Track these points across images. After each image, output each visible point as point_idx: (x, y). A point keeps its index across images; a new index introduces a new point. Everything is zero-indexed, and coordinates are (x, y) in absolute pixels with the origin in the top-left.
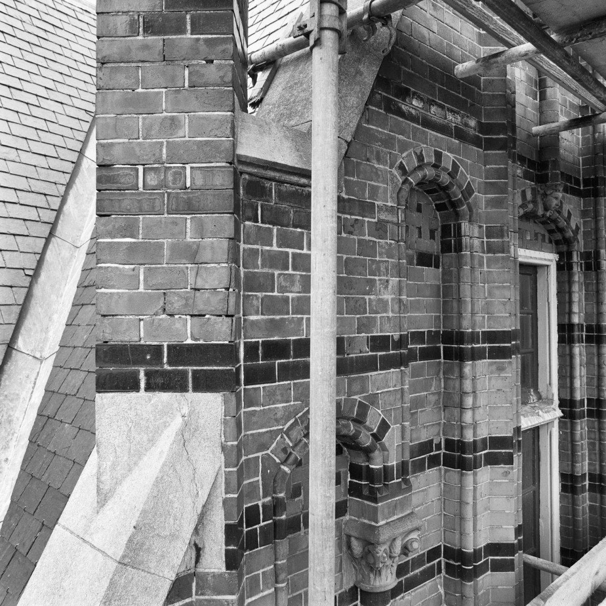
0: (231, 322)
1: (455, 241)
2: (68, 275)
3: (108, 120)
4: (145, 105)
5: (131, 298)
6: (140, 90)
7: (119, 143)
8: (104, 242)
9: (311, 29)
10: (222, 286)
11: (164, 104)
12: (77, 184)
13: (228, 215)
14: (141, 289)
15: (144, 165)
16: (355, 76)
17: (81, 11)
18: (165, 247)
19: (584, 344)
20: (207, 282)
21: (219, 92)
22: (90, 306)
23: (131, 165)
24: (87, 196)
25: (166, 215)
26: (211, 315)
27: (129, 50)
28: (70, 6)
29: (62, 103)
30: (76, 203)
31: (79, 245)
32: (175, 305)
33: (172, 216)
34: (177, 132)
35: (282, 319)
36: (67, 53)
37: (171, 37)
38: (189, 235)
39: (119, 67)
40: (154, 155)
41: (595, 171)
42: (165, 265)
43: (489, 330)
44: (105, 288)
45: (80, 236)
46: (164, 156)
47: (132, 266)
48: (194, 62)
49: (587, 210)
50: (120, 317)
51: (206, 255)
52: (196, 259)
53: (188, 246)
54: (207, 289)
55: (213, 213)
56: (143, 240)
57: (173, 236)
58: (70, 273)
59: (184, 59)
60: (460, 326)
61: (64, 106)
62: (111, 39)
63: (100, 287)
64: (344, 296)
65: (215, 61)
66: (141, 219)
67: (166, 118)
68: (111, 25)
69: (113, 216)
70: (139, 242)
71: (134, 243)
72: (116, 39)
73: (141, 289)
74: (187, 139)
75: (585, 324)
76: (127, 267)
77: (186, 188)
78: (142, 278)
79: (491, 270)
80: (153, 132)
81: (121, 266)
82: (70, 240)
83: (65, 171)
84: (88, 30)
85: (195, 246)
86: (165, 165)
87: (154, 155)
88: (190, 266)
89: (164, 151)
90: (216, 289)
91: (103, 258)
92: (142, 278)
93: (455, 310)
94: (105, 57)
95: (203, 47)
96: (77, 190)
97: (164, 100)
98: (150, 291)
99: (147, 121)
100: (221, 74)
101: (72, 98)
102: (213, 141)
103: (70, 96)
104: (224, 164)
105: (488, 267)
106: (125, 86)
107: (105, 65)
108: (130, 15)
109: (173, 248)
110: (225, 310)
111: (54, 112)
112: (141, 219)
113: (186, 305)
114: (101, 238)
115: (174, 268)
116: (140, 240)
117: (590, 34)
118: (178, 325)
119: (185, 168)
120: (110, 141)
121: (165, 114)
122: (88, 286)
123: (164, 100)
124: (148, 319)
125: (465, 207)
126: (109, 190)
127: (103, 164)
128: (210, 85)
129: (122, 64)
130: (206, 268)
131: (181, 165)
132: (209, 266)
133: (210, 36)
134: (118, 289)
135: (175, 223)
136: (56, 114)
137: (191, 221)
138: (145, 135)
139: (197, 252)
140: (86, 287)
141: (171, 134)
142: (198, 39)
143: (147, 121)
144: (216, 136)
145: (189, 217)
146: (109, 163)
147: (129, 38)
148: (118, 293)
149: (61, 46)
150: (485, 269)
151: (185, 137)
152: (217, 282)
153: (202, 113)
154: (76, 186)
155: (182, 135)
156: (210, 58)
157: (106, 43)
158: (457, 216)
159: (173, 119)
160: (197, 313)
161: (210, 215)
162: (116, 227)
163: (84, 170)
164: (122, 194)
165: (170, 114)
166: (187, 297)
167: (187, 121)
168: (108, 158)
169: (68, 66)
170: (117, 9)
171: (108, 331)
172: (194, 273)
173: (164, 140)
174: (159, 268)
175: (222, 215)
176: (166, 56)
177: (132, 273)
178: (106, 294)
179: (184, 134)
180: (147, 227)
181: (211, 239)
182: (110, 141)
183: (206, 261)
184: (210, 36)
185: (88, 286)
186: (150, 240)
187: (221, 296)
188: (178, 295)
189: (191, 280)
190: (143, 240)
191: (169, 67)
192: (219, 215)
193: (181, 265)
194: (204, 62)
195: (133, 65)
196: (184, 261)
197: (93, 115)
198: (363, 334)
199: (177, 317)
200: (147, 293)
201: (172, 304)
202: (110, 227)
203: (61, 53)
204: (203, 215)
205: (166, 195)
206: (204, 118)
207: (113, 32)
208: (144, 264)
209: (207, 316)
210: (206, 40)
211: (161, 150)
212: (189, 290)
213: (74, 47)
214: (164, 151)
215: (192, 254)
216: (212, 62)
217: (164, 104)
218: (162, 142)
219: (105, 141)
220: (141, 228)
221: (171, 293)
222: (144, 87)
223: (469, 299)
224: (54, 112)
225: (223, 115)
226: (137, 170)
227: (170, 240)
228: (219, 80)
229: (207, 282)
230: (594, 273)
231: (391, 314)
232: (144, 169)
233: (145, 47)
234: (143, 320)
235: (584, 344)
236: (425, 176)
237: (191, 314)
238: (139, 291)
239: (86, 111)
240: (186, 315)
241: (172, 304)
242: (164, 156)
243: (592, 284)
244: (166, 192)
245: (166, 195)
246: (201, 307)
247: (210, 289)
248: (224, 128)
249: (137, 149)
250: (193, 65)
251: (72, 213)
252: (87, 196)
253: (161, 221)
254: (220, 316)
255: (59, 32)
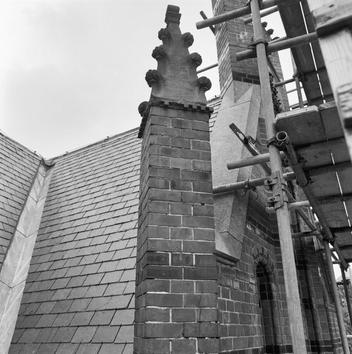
0: (219, 342)
1: (268, 293)
2: (5, 307)
3: (154, 228)
4: (173, 222)
5: (165, 326)
6: (170, 214)
7: (159, 240)
8: (151, 294)
9: (277, 201)
10: (214, 320)
11: (182, 222)
12: (12, 247)
13: (215, 281)
14: (171, 322)
15: (171, 252)
16: (239, 211)
17: (19, 150)
18: (183, 297)
19: (311, 352)
20: (206, 318)
21: (208, 219)
22: (34, 329)
23: (165, 252)
24: (17, 254)
25: (183, 280)
26: (209, 337)
27: (165, 195)
28: (13, 146)
29: (7, 198)
30: (11, 258)
31: (12, 286)
32: (189, 331)
33: (186, 280)
34: (188, 237)
35: (226, 339)
36: (11, 171)
37: (184, 191)
38: (195, 291)
39: (160, 202)
40: (177, 247)
41: (303, 256)
42: (183, 308)
43: (288, 344)
44: (151, 321)
45: (13, 280)
46: (182, 248)
47: (166, 308)
48: (196, 204)
49: (302, 276)
50: (158, 339)
51: (205, 302)
52: (200, 305)
53: (195, 297)
54: (206, 322)
55: (207, 280)
56: (171, 293)
57: (187, 291)
58: (6, 306)
59: (191, 202)
60: (276, 341)
61: (8, 200)
62: (156, 189)
63: (148, 320)
64: (243, 325)
65: (205, 204)
66: (171, 281)
67: (183, 229)
68: (156, 183)
69: (155, 279)
70: (170, 294)
71: (167, 294)
72: (159, 189)
73: (171, 322)
74: (193, 240)
75: (309, 340)
76: (163, 308)
77: (193, 266)
78: (171, 315)
79: (285, 309)
80: (176, 236)
81: (160, 308)
82: (7, 283)
83: (7, 238)
84: (21, 159)
85: (199, 297)
86: (183, 253)
87: (177, 247)
88: (196, 308)
89: (182, 246)
90: (211, 322)
91: (150, 303)
92: (171, 315)
93: (272, 332)
94: (153, 197)
95: (200, 198)
96: (12, 250)
97: (182, 220)
98: (175, 323)
99: (173, 230)
100: (209, 210)
101: (12, 195)
102: (206, 242)
103: (11, 194)
104: (212, 254)
105: (283, 308)
106: (163, 212)
107: (153, 201)
108: (165, 180)
109: (187, 297)
110: (216, 334)
111: (3, 203)
112: (171, 281)
113: (195, 331)
114: (149, 291)
115: (188, 309)
116: (170, 293)
117: (330, 202)
118: (191, 344)
119: (193, 255)
120: (155, 239)
121: (182, 227)
122: (29, 315)
123: (182, 220)
124: (174, 340)
125: (272, 275)
126: (153, 264)
127: (151, 250)
128: (203, 215)
129: (161, 202)
130: (205, 310)
131: (191, 253)
132: (206, 308)
133: (202, 193)
134: (158, 321)
135: (188, 284)
136: (4, 204)
137: (196, 284)
138: (172, 237)
139: (200, 300)
140: (27, 315)
141: (186, 238)
142: (197, 194)
143: (173, 230)
144: (207, 240)
145: (195, 281)
146: (154, 250)
147: (165, 190)
148: (158, 324)
149: (8, 166)
150: (282, 309)
151: (192, 239)
152: (211, 318)
153: (200, 228)
154: (11, 248)
155: (191, 238)
156: (203, 202)
157: (154, 191)
158: (268, 280)
159: (186, 230)
160: (201, 336)
161: (205, 281)
162: (158, 285)
163: (16, 238)
164: (160, 267)
165: (185, 227)
166: (196, 326)
167: (193, 231)
168: (154, 248)
169: (11, 178)
170: (159, 176)
171: (152, 348)
172: (199, 312)
173: (182, 240)
174: (180, 309)
175: (212, 281)
176: (183, 200)
177: (165, 312)
178: (151, 324)
179: (192, 238)
180: (173, 286)
181: (207, 294)
182: (155, 239)
183: (204, 306)
184: (202, 193)
185: (29, 315)
186: (176, 293)
187: (213, 326)
188: (191, 325)
189: (197, 316)
190: (171, 293)
191: (184, 205)
192: (210, 281)
193: (192, 308)
194: (200, 204)
195: (167, 202)
196: (193, 305)
197: (22, 206)
198: (251, 348)
199: (190, 338)
200: (174, 324)
201: (188, 330)
202: (154, 285)
203: (8, 170)
204: (202, 281)
205: (183, 269)
206: (201, 230)
207: (157, 186)
208: (172, 307)
209: (206, 338)
210: (201, 194)
211: (181, 245)
212: (196, 322)
213: (15, 168)
214: (182, 246)
215: (198, 302)
216: (204, 204)
217: (182, 222)
218: (181, 241)
219: (152, 239)
220: (170, 286)
221: (187, 324)
222: (172, 213)
223: (279, 326)
224: (3, 203)
225: (210, 230)
226: (168, 254)
227: (186, 294)
228: (208, 213)
229: (206, 318)
230: (310, 310)
231: (258, 336)
232: (172, 254)
233: (172, 195)
234: (171, 340)
235: (311, 352)
236: (260, 259)
237: (198, 336)
238: (170, 322)
239: (19, 203)
240: (195, 337)
241: (188, 330)
242: (182, 248)
243: (310, 316)
244: (183, 267)
245: (183, 269)
246: (203, 332)
247: (208, 322)
248: (211, 236)
249: (169, 244)
250: (195, 205)
251: (9, 265)
252: (17, 254)
253: (181, 283)
254: (213, 338)
255: (8, 159)
